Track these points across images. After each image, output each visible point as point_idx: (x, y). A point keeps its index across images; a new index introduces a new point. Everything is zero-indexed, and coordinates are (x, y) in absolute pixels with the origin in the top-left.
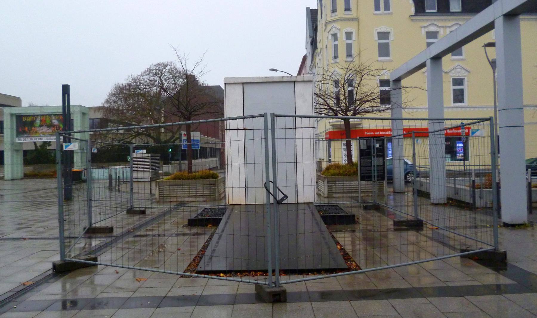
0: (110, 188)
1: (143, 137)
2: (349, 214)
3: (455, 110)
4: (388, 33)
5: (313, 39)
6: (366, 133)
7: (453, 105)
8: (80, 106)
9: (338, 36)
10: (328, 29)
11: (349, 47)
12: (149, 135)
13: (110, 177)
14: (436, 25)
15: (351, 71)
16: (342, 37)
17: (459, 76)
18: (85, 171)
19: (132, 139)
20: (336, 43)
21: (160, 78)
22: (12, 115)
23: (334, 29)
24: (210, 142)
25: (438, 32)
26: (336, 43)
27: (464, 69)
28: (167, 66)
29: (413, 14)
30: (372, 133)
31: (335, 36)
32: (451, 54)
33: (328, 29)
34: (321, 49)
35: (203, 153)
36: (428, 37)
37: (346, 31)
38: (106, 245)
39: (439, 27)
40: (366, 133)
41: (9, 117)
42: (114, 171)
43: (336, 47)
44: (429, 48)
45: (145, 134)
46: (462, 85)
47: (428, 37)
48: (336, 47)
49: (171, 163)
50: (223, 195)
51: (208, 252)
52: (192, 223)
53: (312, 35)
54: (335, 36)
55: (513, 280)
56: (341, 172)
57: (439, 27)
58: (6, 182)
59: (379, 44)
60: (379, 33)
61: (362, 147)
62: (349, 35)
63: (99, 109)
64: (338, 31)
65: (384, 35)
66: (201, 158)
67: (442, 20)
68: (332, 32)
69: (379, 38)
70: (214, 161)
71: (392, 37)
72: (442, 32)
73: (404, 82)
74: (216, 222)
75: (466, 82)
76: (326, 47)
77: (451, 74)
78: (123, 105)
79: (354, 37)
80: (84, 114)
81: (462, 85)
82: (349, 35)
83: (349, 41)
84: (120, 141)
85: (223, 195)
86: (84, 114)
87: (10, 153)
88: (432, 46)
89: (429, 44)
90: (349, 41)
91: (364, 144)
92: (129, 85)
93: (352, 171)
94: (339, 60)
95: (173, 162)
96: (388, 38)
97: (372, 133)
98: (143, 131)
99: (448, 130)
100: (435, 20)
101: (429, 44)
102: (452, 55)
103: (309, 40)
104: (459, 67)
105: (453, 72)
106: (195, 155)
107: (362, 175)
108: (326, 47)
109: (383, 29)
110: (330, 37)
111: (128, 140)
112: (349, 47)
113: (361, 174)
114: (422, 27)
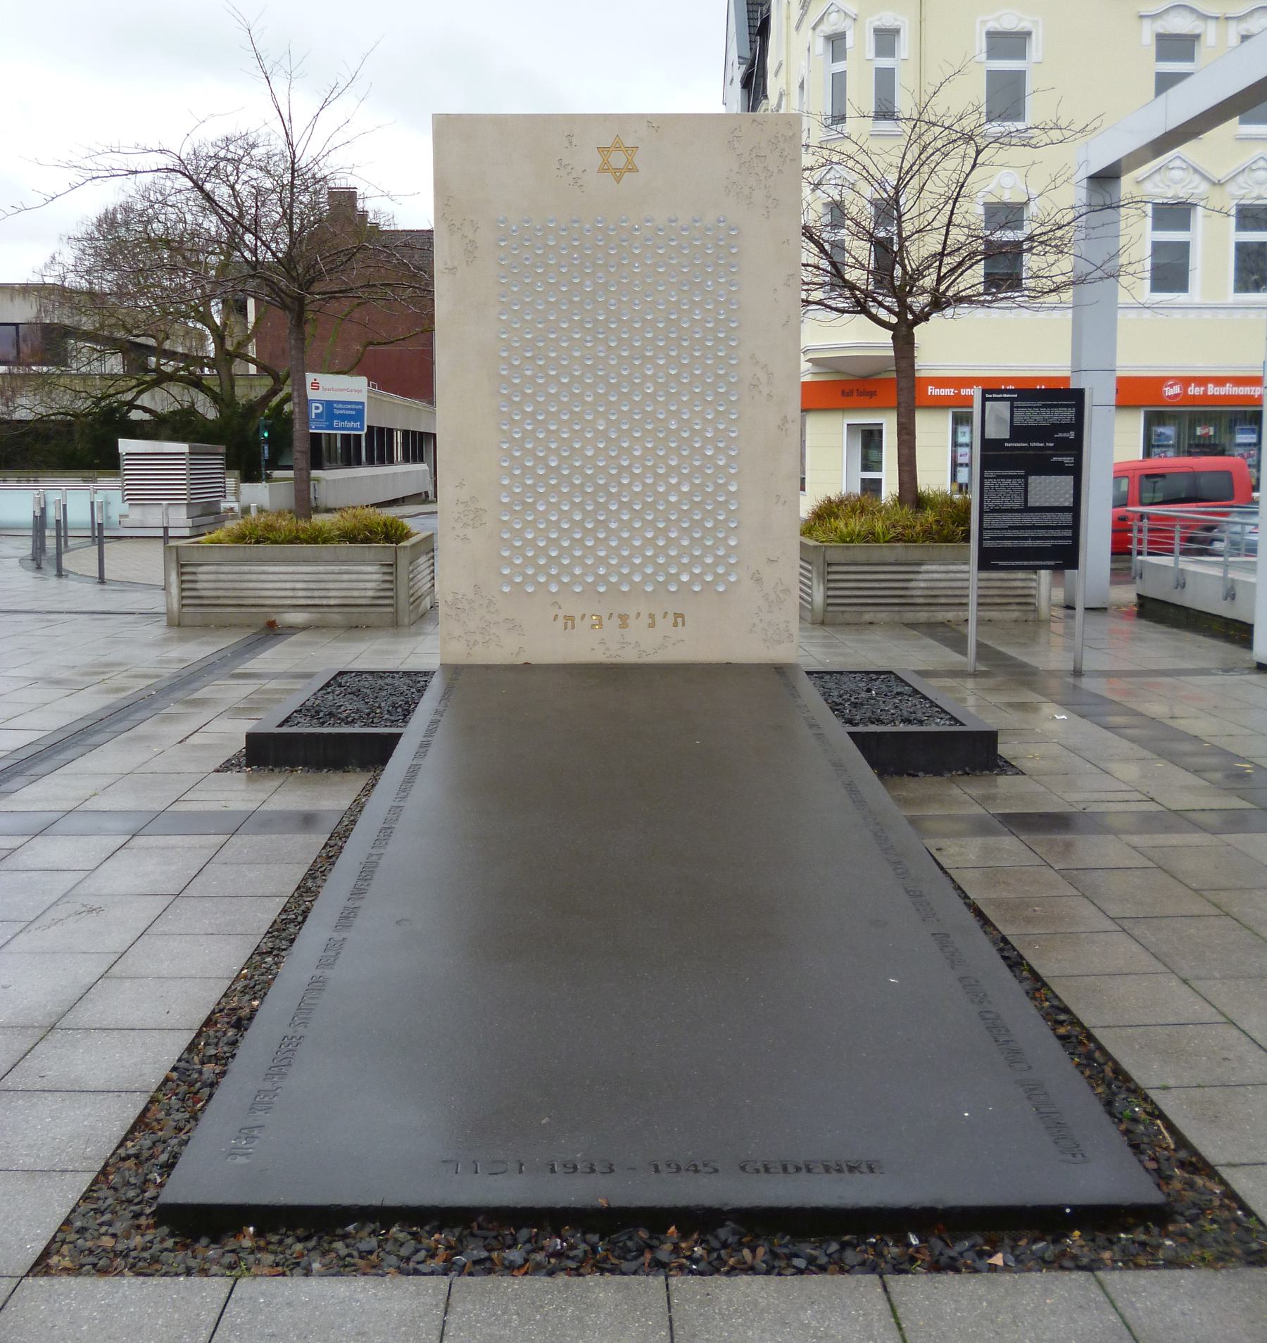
0: (37, 560)
1: (176, 389)
2: (971, 727)
3: (1238, 315)
4: (1194, 38)
5: (752, 65)
6: (932, 390)
7: (1233, 297)
9: (849, 42)
10: (813, 16)
11: (885, 80)
12: (197, 383)
13: (40, 522)
15: (937, 130)
16: (861, 45)
17: (1258, 198)
19: (140, 393)
20: (839, 67)
21: (233, 188)
23: (834, 17)
24: (398, 413)
25: (1198, 36)
26: (839, 67)
27: (1196, 171)
28: (254, 146)
30: (949, 392)
31: (836, 43)
33: (813, 16)
34: (781, 95)
35: (378, 446)
36: (1162, 55)
37: (877, 24)
39: (1206, 17)
40: (932, 390)
43: (839, 81)
44: (1163, 96)
45: (181, 379)
46: (1186, 226)
47: (1162, 55)
48: (839, 81)
49: (268, 478)
50: (427, 603)
51: (272, 1015)
52: (265, 753)
53: (748, 54)
54: (836, 43)
56: (879, 527)
57: (1206, 17)
59: (991, 74)
60: (992, 35)
61: (991, 434)
62: (886, 39)
63: (25, 290)
64: (849, 22)
65: (1008, 43)
66: (371, 462)
68: (827, 28)
69: (992, 53)
70: (401, 475)
71: (1035, 49)
73: (1127, 184)
74: (372, 753)
76: (802, 86)
77: (1232, 188)
78: (107, 282)
79: (905, 46)
82: (886, 39)
83: (885, 62)
84: (100, 400)
85: (427, 603)
88: (1174, 92)
89: (1165, 82)
90: (885, 62)
91: (999, 419)
92: (127, 209)
93: (918, 528)
94: (849, 127)
95: (277, 474)
96: (1021, 54)
97: (949, 392)
98: (178, 369)
99: (1210, 386)
101: (1165, 82)
102: (1242, 122)
103: (738, 73)
105: (1241, 179)
106: (320, 453)
107: (987, 544)
108: (802, 86)
109: (1009, 22)
110: (820, 46)
111: (128, 397)
112: (885, 80)
113: (981, 539)
114: (1141, 17)
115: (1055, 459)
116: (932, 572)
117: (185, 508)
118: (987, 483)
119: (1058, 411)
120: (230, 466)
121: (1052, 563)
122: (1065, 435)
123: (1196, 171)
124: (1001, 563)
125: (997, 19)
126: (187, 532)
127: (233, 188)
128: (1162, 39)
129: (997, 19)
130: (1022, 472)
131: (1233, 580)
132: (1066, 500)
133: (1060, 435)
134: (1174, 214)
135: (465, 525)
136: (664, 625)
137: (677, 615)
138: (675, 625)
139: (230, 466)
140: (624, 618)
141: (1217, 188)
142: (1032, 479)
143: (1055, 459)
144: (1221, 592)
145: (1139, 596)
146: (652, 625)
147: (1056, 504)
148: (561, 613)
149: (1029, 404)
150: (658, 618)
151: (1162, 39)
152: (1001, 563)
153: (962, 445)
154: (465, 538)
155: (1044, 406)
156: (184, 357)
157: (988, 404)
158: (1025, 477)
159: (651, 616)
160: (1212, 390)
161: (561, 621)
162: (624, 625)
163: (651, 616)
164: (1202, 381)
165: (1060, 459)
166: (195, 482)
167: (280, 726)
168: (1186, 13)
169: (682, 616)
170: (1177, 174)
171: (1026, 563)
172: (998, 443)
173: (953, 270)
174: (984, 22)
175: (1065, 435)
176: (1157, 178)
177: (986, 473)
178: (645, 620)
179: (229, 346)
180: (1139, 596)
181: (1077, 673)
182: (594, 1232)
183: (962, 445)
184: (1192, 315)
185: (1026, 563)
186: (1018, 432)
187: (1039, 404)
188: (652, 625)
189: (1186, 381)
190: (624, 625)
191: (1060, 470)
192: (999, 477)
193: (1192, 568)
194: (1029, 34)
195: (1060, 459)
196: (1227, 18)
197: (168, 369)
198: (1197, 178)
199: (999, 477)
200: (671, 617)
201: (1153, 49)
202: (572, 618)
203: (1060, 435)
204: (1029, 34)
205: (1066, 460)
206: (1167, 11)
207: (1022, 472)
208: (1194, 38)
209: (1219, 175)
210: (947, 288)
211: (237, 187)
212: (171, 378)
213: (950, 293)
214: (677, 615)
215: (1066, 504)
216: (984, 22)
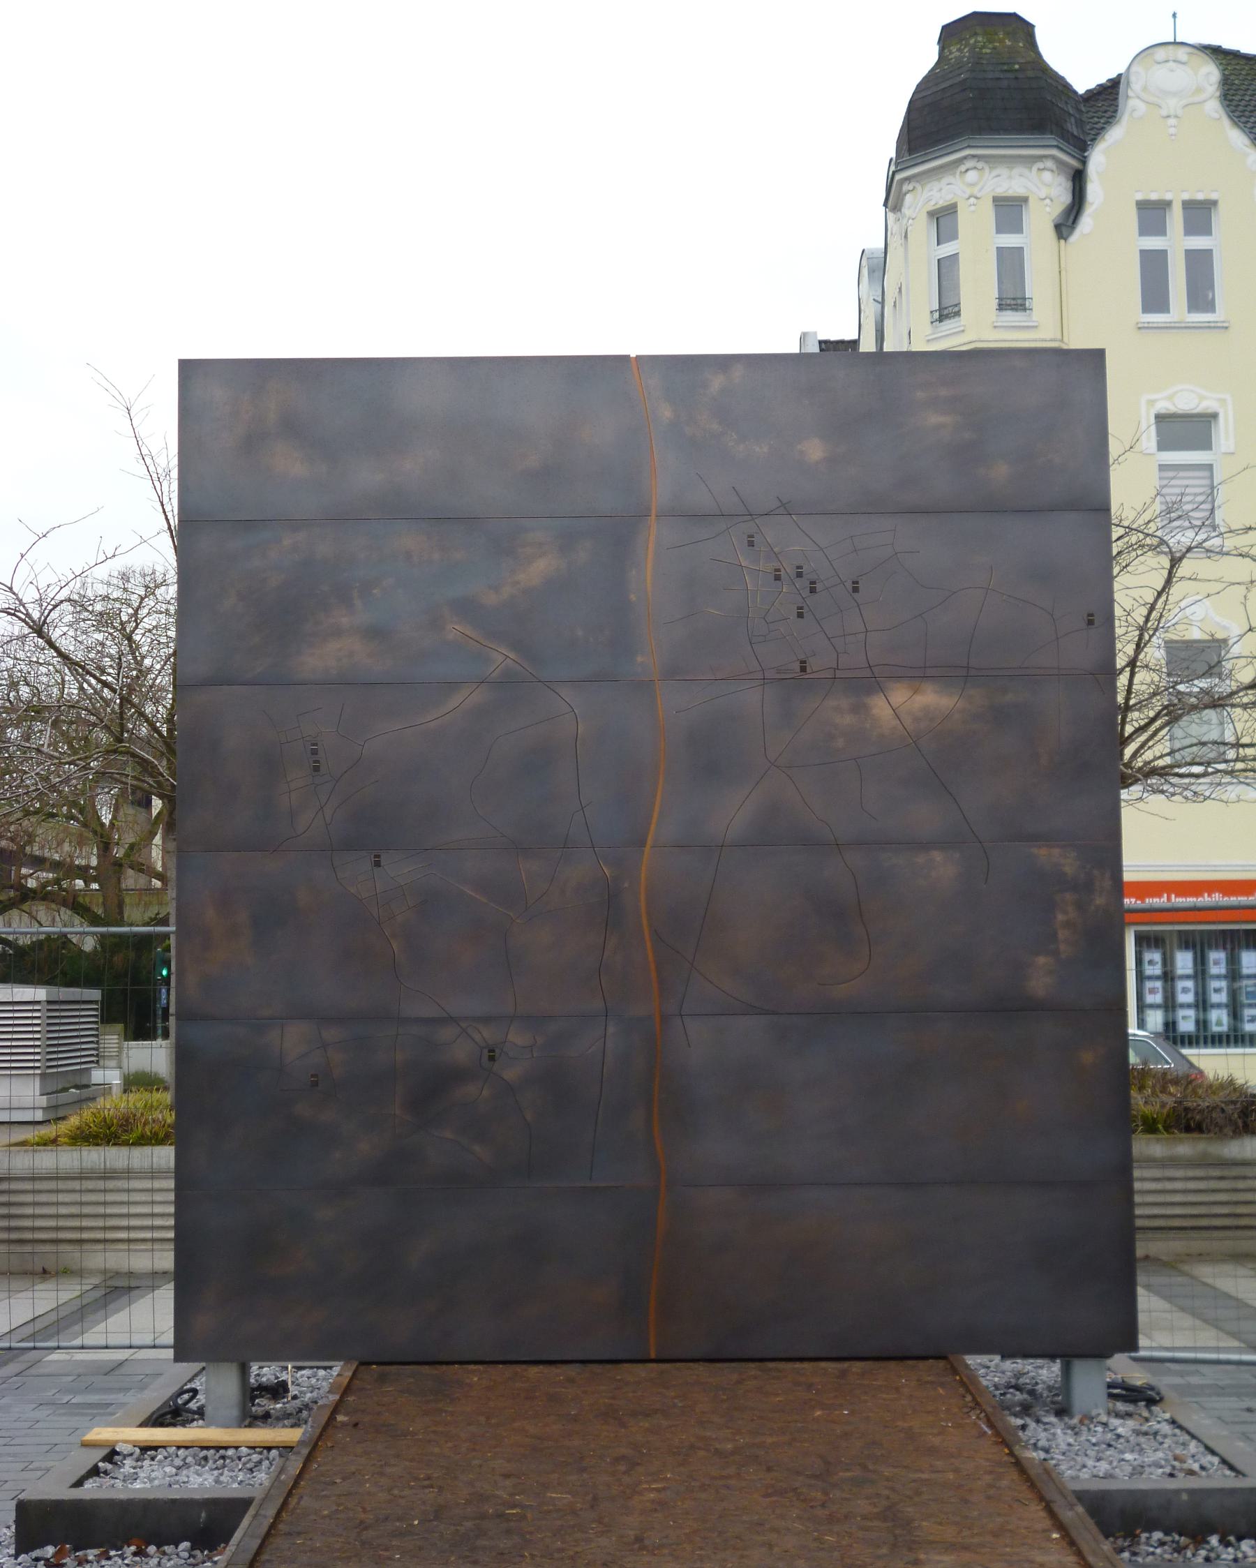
1: (41, 911)
20: (947, 249)
26: (947, 249)
43: (946, 269)
48: (946, 269)
71: (1224, 436)
109: (1186, 402)
116: (1227, 1191)
117: (38, 1080)
120: (109, 1015)
125: (1170, 398)
126: (39, 1116)
127: (129, 638)
129: (1170, 398)
139: (109, 1015)
153: (1150, 978)
156: (56, 866)
166: (55, 1045)
173: (1140, 730)
174: (1151, 403)
179: (118, 852)
182: (1111, 568)
183: (1150, 978)
194: (1214, 416)
197: (32, 883)
204: (1214, 416)
210: (1135, 755)
211: (137, 638)
212: (40, 895)
213: (1139, 763)
216: (1151, 403)
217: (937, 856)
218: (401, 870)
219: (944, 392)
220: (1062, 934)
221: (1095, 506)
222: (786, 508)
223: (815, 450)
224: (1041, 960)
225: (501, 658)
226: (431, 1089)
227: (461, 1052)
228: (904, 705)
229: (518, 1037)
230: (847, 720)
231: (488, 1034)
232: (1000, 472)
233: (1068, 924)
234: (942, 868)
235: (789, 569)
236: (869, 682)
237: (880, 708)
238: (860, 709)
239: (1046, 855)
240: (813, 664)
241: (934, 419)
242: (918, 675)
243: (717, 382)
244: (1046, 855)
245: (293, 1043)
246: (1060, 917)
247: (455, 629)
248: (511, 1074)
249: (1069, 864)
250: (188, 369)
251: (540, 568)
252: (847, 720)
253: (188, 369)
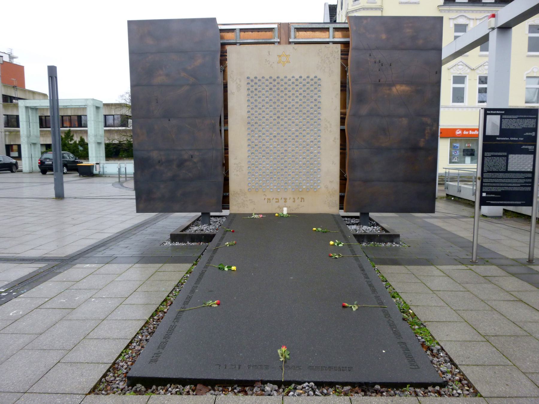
4: (466, 25)
7: (451, 104)
8: (93, 99)
14: (466, 17)
18: (98, 166)
22: (27, 108)
25: (467, 25)
27: (466, 66)
29: (442, 4)
32: (479, 48)
36: (456, 31)
38: (187, 228)
39: (470, 19)
41: (24, 110)
42: (123, 165)
46: (463, 83)
47: (456, 31)
55: (532, 269)
57: (470, 19)
58: (24, 175)
61: (489, 132)
67: (473, 11)
72: (471, 25)
75: (467, 80)
80: (97, 108)
81: (463, 83)
86: (97, 108)
87: (26, 146)
100: (465, 11)
101: (456, 37)
102: (481, 50)
104: (461, 63)
105: (480, 68)
115: (523, 147)
118: (486, 159)
119: (526, 121)
121: (520, 203)
122: (530, 134)
123: (466, 66)
124: (492, 202)
128: (456, 25)
130: (505, 154)
131: (460, 186)
132: (529, 168)
133: (527, 134)
134: (459, 79)
135: (237, 171)
136: (298, 201)
137: (302, 198)
138: (301, 201)
140: (285, 199)
141: (473, 72)
142: (510, 156)
143: (523, 147)
144: (456, 189)
145: (447, 195)
146: (294, 201)
147: (523, 170)
148: (266, 198)
149: (510, 117)
150: (296, 199)
151: (456, 25)
152: (492, 202)
154: (237, 175)
155: (518, 118)
157: (488, 117)
158: (507, 157)
159: (294, 199)
160: (471, 132)
161: (266, 200)
162: (285, 202)
163: (294, 199)
164: (468, 130)
165: (526, 147)
167: (181, 231)
168: (464, 18)
169: (303, 198)
170: (460, 67)
171: (512, 202)
172: (493, 138)
175: (530, 134)
176: (454, 68)
177: (486, 154)
178: (292, 200)
180: (447, 195)
181: (530, 261)
184: (465, 109)
185: (505, 202)
186: (503, 132)
187: (516, 117)
188: (294, 201)
189: (463, 130)
190: (285, 202)
191: (527, 152)
192: (492, 156)
193: (463, 186)
195: (526, 147)
196: (476, 19)
198: (467, 68)
199: (492, 156)
200: (300, 199)
201: (454, 29)
202: (269, 199)
203: (527, 134)
205: (530, 147)
206: (458, 17)
207: (505, 154)
208: (466, 25)
209: (473, 67)
214: (302, 198)
215: (529, 170)
217: (404, 119)
218: (174, 122)
219: (410, 25)
220: (427, 135)
221: (439, 49)
222: (378, 48)
223: (384, 36)
224: (422, 140)
225: (192, 80)
226: (181, 164)
227: (186, 157)
228: (399, 89)
229: (196, 153)
230: (388, 92)
231: (191, 153)
232: (421, 42)
233: (428, 133)
234: (405, 121)
235: (378, 61)
236: (391, 85)
237: (394, 89)
238: (390, 89)
239: (424, 119)
240: (381, 80)
241: (408, 30)
242: (402, 83)
243: (365, 22)
244: (424, 119)
245: (155, 155)
246: (426, 131)
247: (183, 74)
248: (195, 160)
249: (429, 121)
250: (130, 23)
251: (199, 62)
252: (388, 92)
253: (130, 23)
